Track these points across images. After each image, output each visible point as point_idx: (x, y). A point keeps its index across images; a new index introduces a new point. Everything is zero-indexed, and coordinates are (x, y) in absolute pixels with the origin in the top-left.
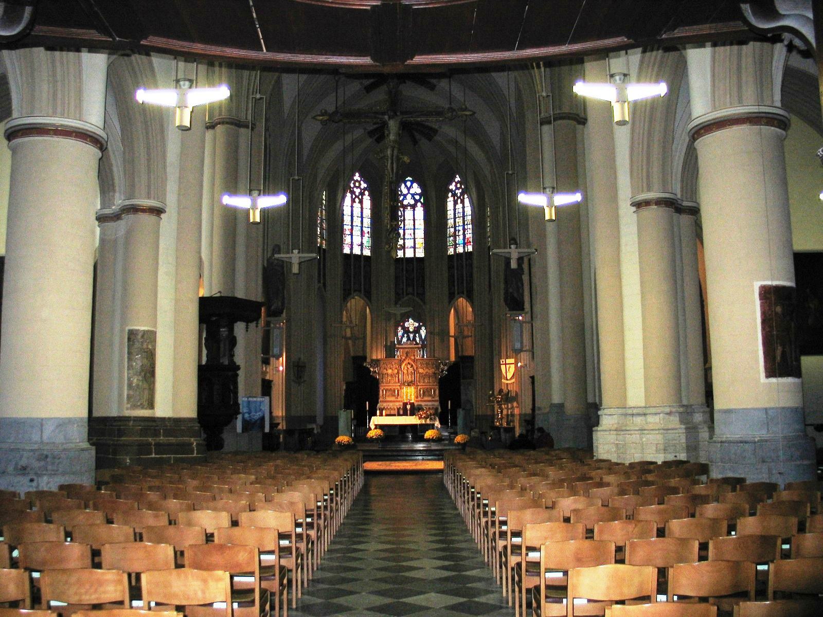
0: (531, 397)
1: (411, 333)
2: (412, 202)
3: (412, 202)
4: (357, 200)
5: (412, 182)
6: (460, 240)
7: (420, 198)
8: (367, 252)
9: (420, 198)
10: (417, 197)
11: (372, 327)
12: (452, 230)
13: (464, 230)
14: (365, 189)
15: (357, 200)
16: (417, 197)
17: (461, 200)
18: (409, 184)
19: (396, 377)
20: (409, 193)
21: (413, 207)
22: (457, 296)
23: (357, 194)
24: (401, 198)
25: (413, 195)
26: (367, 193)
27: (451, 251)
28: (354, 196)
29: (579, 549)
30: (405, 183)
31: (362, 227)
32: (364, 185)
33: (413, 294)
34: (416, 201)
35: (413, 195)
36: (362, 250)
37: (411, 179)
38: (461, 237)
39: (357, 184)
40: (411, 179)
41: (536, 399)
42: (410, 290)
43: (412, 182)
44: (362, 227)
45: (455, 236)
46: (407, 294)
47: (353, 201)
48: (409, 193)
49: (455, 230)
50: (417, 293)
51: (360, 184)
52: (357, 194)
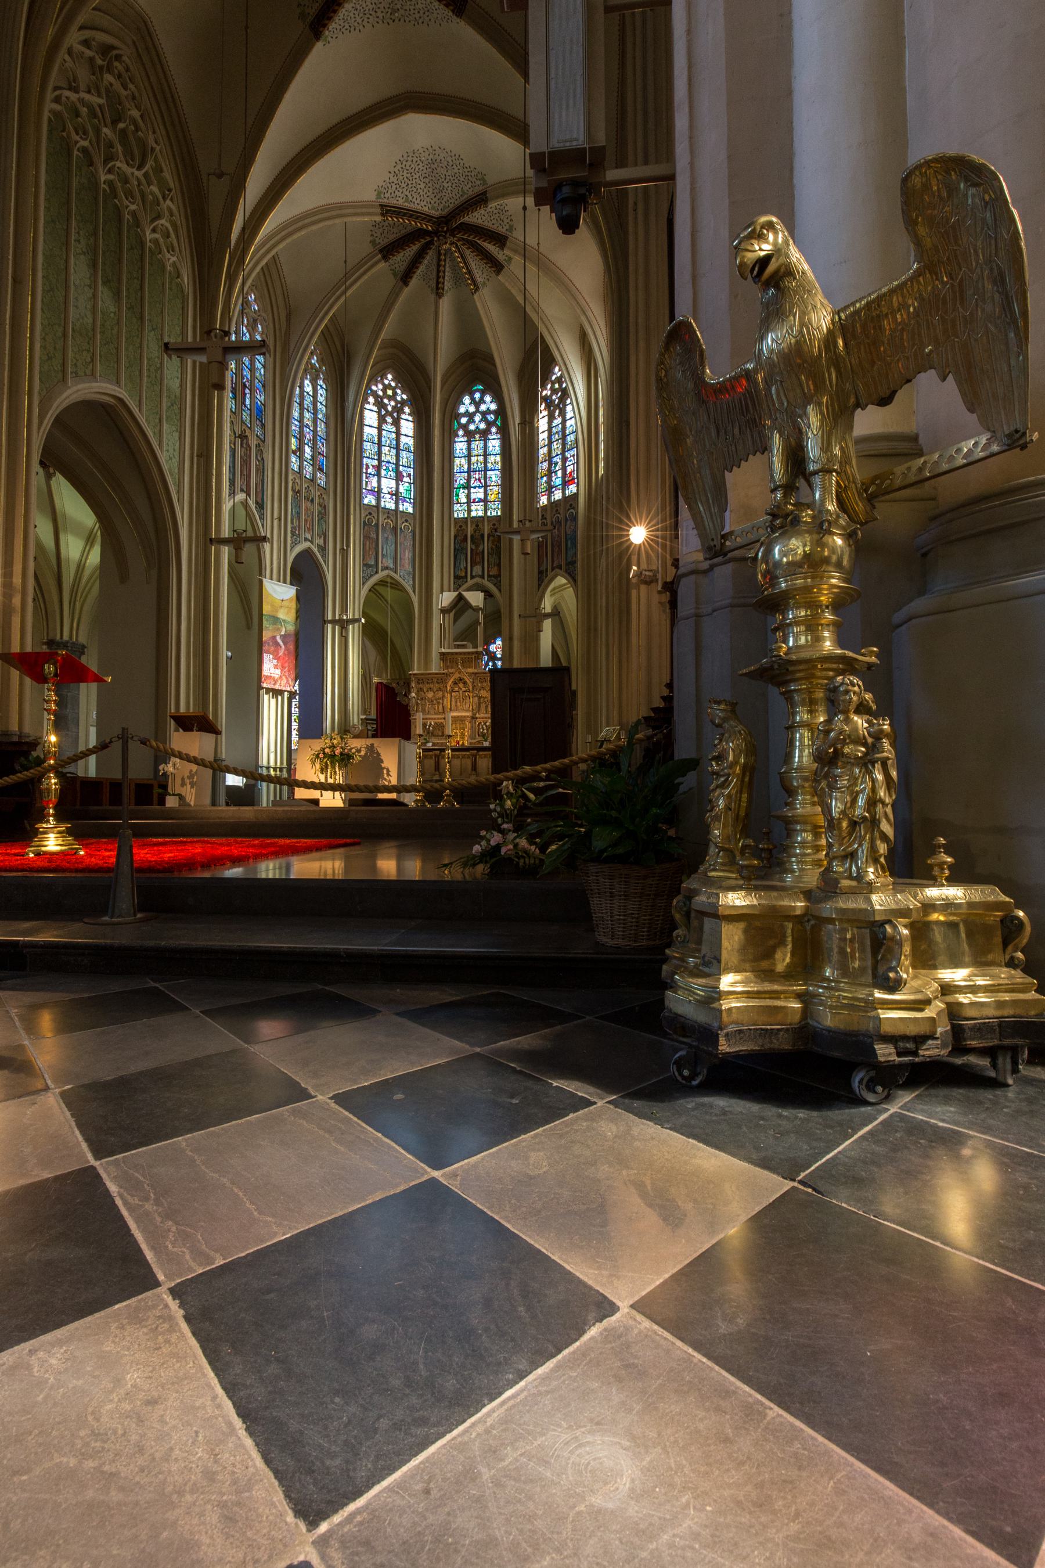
0: (669, 670)
1: (499, 659)
2: (482, 426)
3: (482, 426)
4: (389, 420)
5: (483, 393)
6: (557, 481)
7: (496, 419)
8: (408, 507)
9: (496, 419)
10: (491, 417)
11: (992, 1270)
12: (545, 465)
13: (565, 460)
14: (403, 403)
15: (389, 420)
16: (491, 417)
17: (560, 410)
18: (477, 396)
19: (439, 703)
20: (477, 410)
21: (485, 434)
22: (550, 574)
23: (390, 408)
24: (464, 420)
25: (484, 414)
26: (407, 410)
27: (544, 500)
28: (383, 412)
29: (927, 1156)
30: (471, 395)
31: (397, 465)
32: (402, 396)
33: (483, 577)
34: (489, 424)
35: (484, 414)
36: (397, 504)
37: (481, 387)
38: (560, 474)
39: (390, 392)
40: (481, 387)
41: (667, 292)
42: (477, 569)
43: (483, 393)
44: (397, 465)
45: (550, 473)
46: (472, 577)
47: (382, 420)
48: (477, 410)
49: (550, 464)
50: (489, 576)
51: (395, 394)
52: (390, 408)
